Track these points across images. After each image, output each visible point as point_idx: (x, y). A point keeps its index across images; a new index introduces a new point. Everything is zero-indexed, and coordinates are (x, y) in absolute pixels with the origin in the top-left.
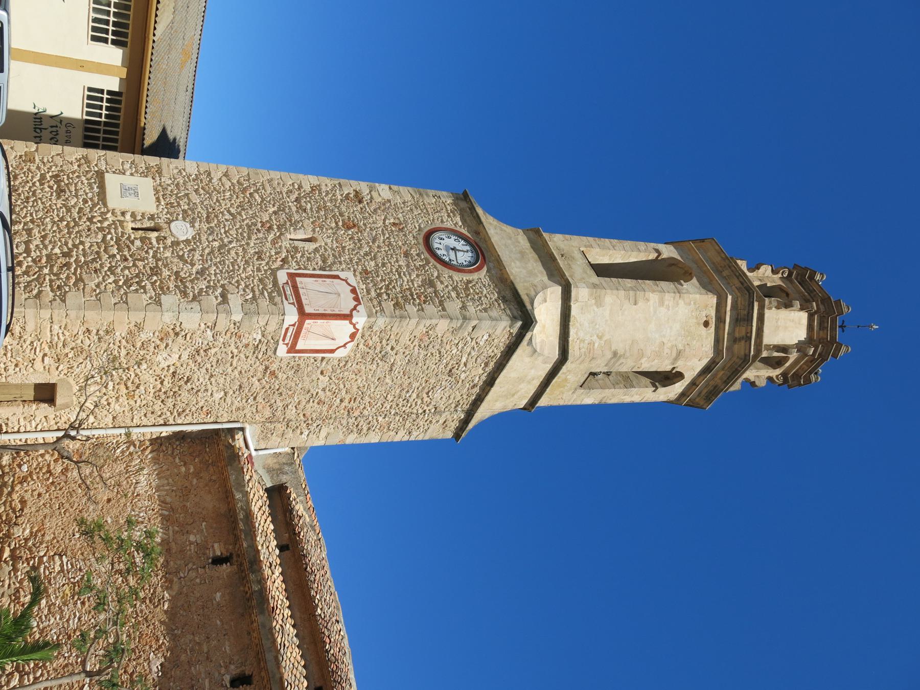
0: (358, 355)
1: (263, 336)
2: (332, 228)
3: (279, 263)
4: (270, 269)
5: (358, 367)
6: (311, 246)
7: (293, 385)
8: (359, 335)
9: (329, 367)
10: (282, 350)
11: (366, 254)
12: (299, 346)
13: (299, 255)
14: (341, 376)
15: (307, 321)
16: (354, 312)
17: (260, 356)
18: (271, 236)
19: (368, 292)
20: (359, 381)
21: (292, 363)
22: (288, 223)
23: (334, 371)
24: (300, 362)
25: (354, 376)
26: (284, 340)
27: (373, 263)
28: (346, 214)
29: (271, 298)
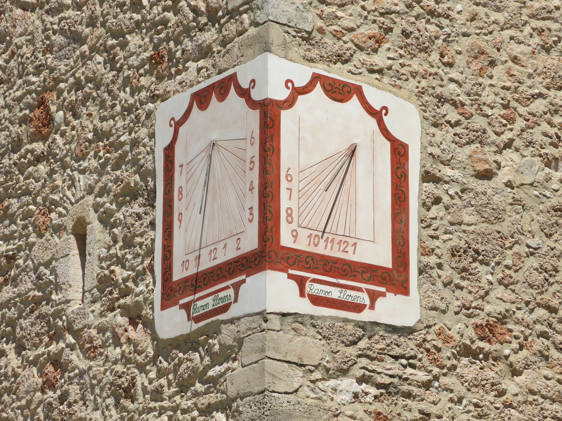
0: (415, 65)
1: (344, 372)
2: (52, 172)
3: (138, 334)
4: (154, 361)
5: (460, 61)
6: (97, 233)
7: (533, 262)
8: (339, 73)
9: (463, 154)
10: (395, 309)
11: (111, 62)
12: (381, 255)
13: (120, 273)
14: (498, 112)
15: (286, 240)
16: (256, 95)
17: (422, 376)
18: (77, 359)
19: (205, 52)
20: (517, 50)
21: (447, 273)
22: (46, 309)
23: (480, 138)
24: (443, 249)
25: (498, 71)
26: (358, 308)
27: (134, 40)
28: (15, 129)
29: (227, 354)
